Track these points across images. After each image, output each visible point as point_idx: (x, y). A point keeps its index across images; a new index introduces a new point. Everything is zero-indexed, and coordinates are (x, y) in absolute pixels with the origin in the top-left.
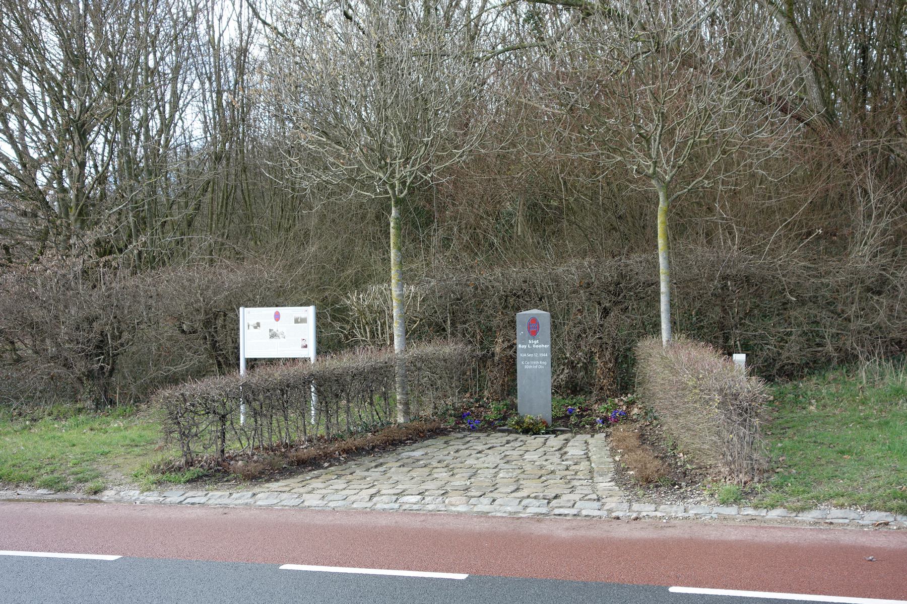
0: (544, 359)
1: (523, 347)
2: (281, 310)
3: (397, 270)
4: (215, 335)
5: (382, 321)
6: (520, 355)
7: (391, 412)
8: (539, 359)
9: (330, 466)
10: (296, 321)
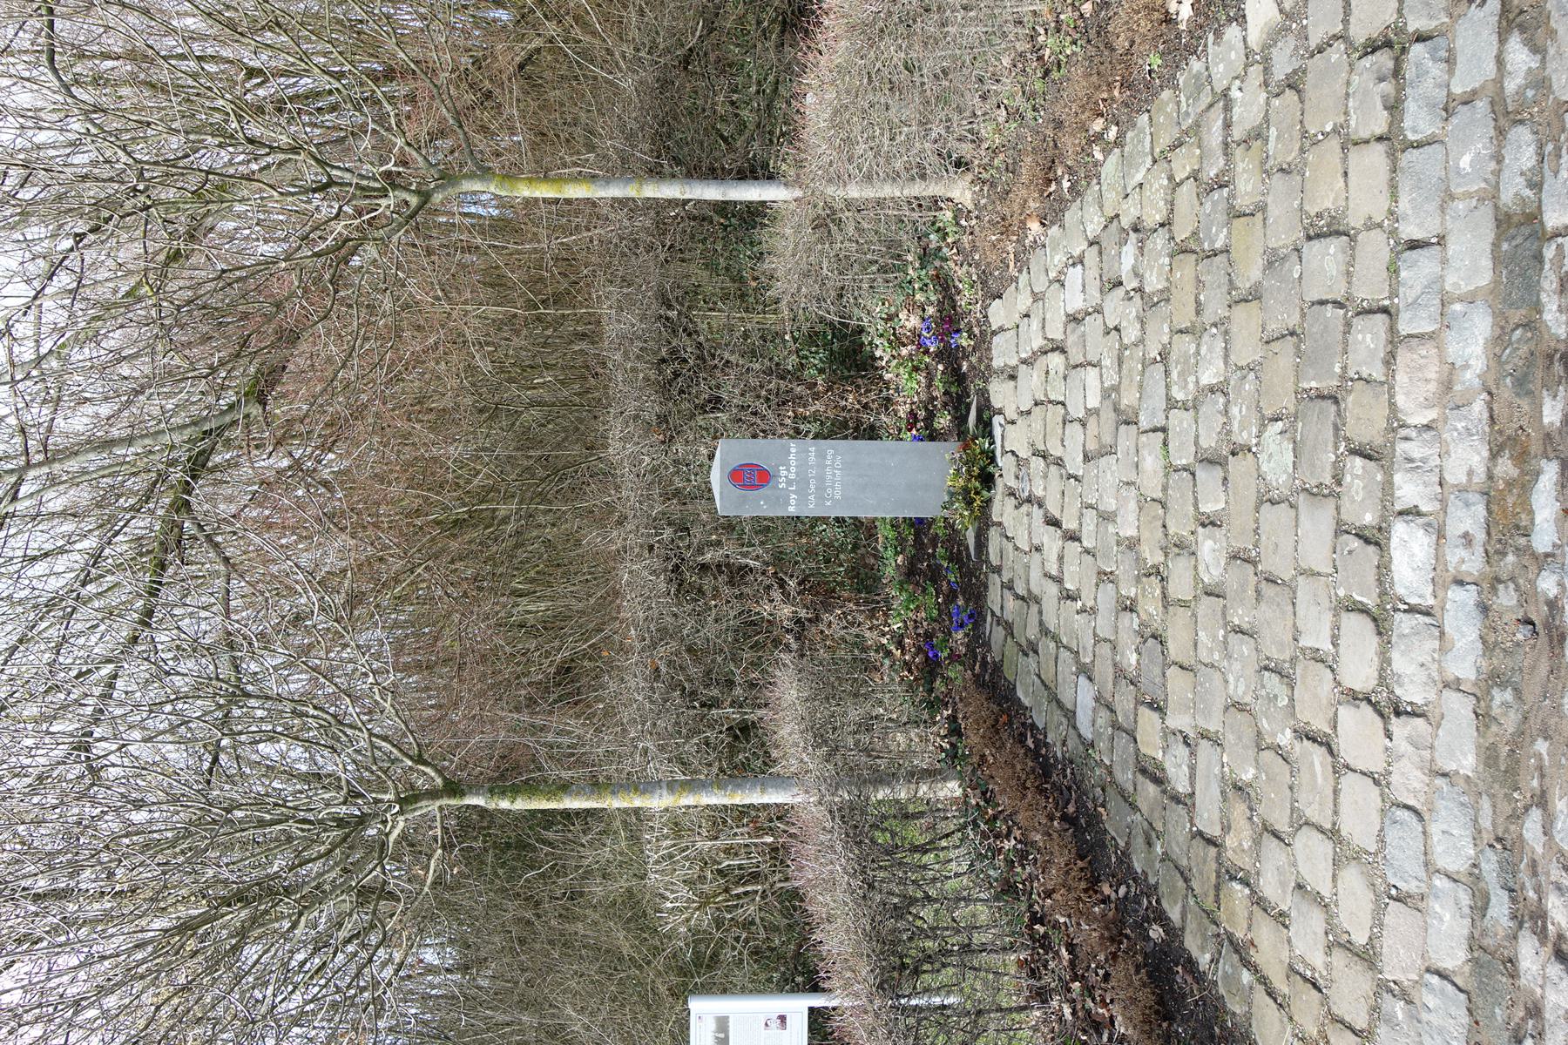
0: (821, 455)
1: (793, 502)
6: (811, 509)
7: (933, 809)
9: (1161, 918)
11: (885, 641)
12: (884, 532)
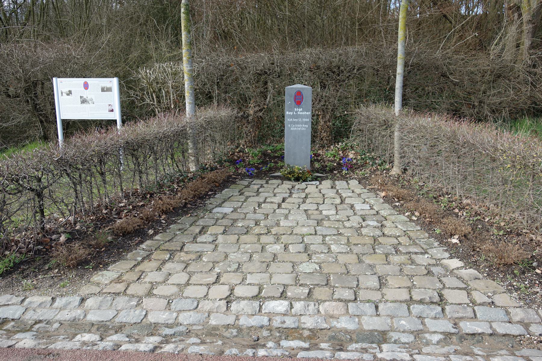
0: (306, 123)
1: (290, 113)
2: (89, 80)
3: (188, 50)
4: (35, 99)
5: (166, 90)
6: (287, 120)
7: (186, 160)
8: (302, 123)
9: (156, 233)
10: (103, 90)
11: (241, 146)
12: (279, 146)
